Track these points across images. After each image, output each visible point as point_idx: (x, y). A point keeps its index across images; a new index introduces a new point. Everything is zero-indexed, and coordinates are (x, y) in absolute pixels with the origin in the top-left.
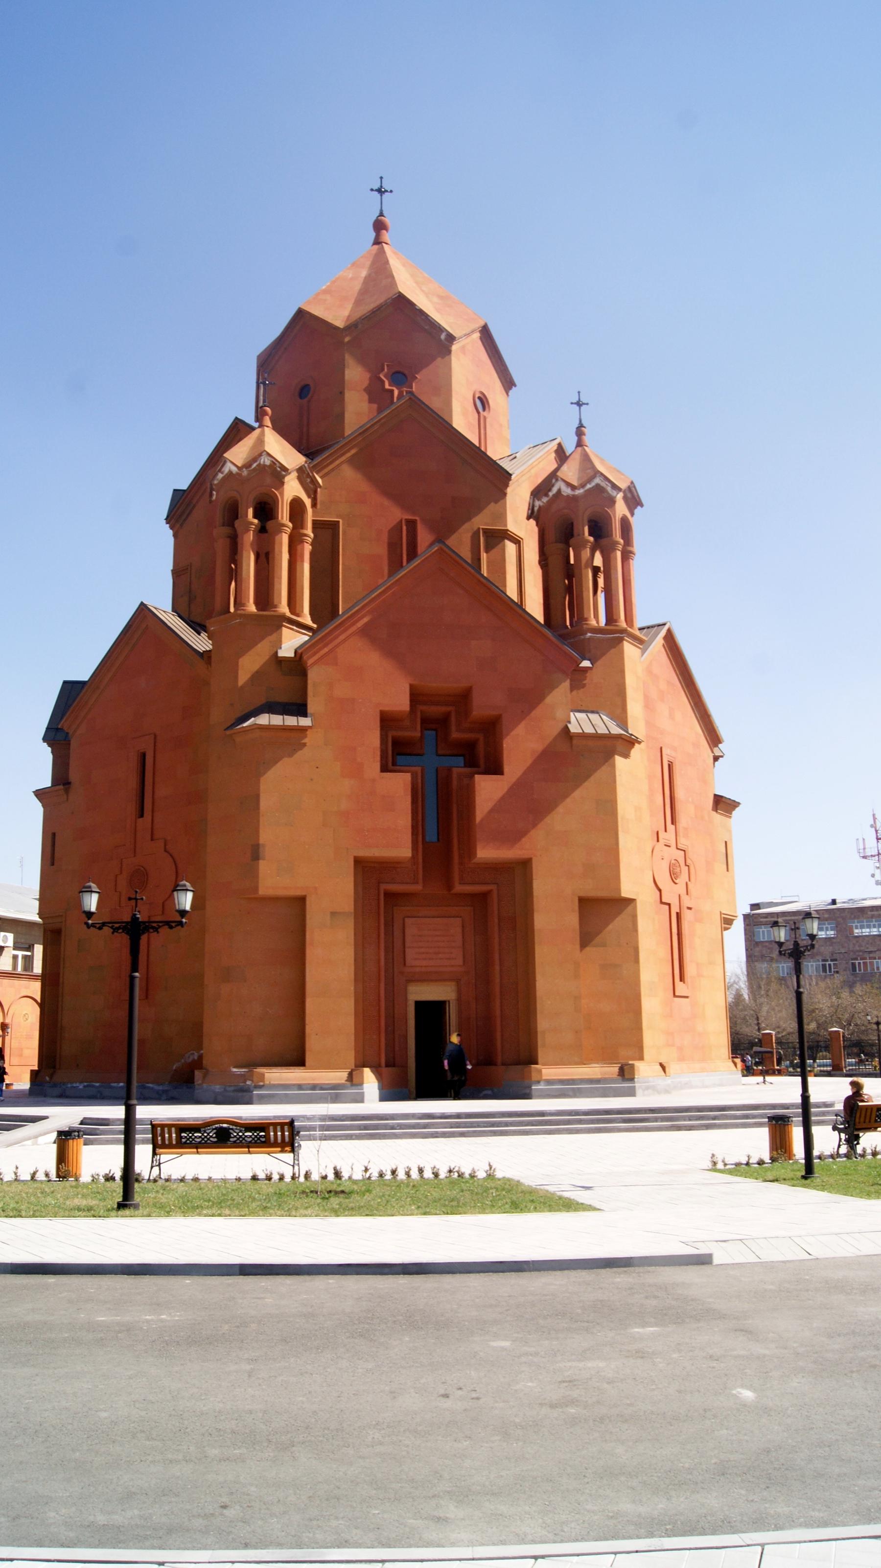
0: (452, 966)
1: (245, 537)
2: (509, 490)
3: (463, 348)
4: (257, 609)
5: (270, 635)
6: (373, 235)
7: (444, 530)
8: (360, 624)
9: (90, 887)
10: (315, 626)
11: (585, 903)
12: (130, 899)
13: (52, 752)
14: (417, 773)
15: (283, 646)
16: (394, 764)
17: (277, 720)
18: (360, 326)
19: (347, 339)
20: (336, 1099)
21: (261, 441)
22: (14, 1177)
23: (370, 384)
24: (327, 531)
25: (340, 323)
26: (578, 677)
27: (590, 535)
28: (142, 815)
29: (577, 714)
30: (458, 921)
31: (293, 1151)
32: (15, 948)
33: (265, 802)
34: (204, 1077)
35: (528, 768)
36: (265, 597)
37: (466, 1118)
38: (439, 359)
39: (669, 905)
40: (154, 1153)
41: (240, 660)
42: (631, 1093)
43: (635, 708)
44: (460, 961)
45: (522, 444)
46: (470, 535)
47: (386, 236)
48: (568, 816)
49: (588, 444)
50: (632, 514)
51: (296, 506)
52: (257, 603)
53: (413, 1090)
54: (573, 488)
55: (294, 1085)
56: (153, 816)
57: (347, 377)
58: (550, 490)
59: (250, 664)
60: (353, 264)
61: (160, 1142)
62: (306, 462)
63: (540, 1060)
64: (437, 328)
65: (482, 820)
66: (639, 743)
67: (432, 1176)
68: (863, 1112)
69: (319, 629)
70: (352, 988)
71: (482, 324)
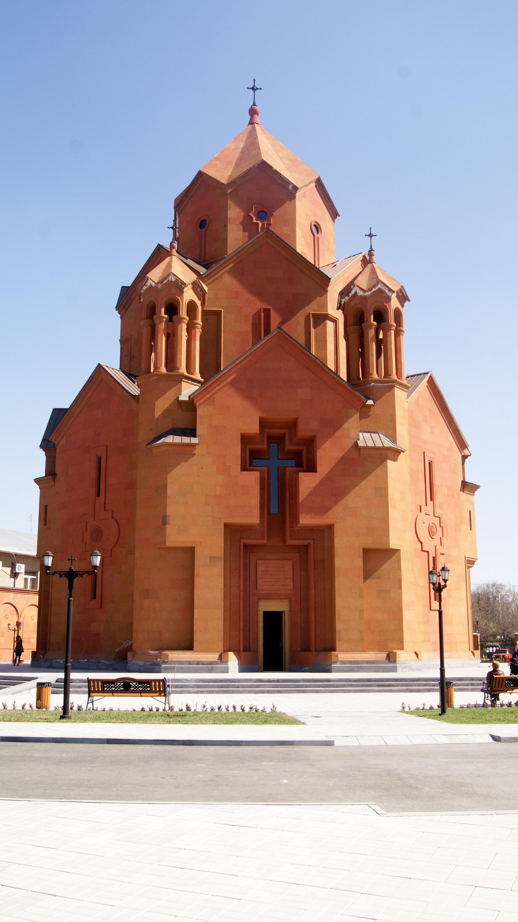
0: (286, 590)
1: (160, 326)
2: (329, 288)
3: (304, 195)
4: (167, 370)
5: (175, 386)
6: (249, 117)
7: (287, 315)
8: (229, 380)
9: (48, 553)
10: (203, 380)
11: (367, 552)
12: (68, 559)
13: (46, 454)
14: (264, 471)
15: (182, 393)
16: (250, 465)
17: (177, 439)
18: (237, 182)
19: (229, 191)
20: (211, 671)
21: (169, 266)
22: (13, 707)
23: (243, 220)
24: (213, 319)
25: (224, 181)
26: (365, 411)
27: (374, 321)
28: (99, 495)
29: (365, 434)
30: (290, 562)
31: (165, 695)
32: (27, 573)
33: (171, 490)
34: (133, 656)
35: (333, 468)
36: (171, 361)
37: (282, 682)
38: (288, 202)
39: (428, 552)
40: (89, 696)
41: (156, 402)
42: (394, 670)
43: (402, 429)
44: (291, 587)
45: (337, 259)
46: (304, 317)
47: (257, 119)
48: (356, 498)
49: (375, 262)
50: (403, 306)
51: (191, 306)
52: (166, 367)
53: (262, 666)
54: (364, 291)
55: (186, 662)
56: (105, 496)
57: (229, 216)
58: (350, 292)
59: (162, 404)
60: (235, 139)
61: (92, 689)
62: (197, 278)
63: (337, 649)
64: (285, 182)
65: (303, 500)
66: (403, 452)
67: (241, 711)
68: (497, 681)
69: (206, 381)
70: (222, 603)
71: (317, 177)
